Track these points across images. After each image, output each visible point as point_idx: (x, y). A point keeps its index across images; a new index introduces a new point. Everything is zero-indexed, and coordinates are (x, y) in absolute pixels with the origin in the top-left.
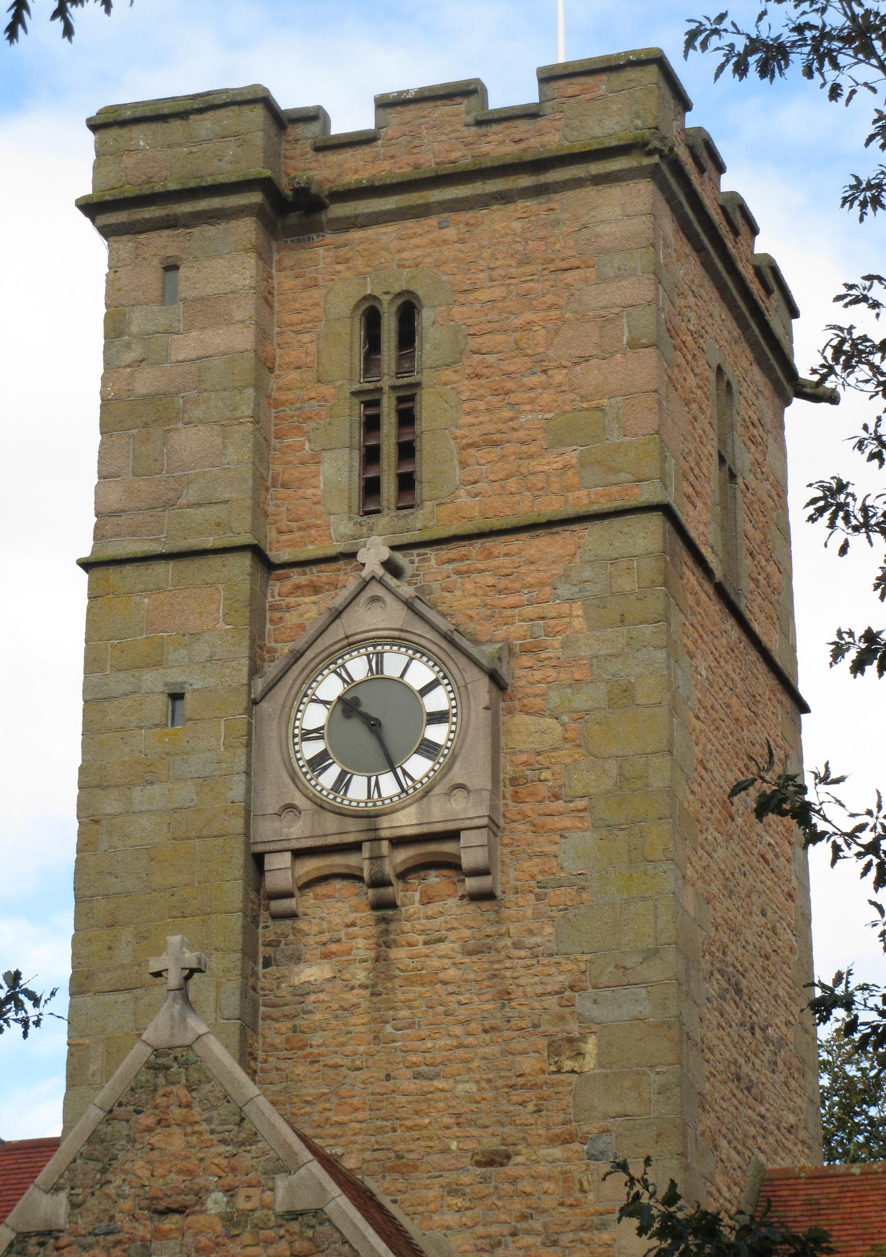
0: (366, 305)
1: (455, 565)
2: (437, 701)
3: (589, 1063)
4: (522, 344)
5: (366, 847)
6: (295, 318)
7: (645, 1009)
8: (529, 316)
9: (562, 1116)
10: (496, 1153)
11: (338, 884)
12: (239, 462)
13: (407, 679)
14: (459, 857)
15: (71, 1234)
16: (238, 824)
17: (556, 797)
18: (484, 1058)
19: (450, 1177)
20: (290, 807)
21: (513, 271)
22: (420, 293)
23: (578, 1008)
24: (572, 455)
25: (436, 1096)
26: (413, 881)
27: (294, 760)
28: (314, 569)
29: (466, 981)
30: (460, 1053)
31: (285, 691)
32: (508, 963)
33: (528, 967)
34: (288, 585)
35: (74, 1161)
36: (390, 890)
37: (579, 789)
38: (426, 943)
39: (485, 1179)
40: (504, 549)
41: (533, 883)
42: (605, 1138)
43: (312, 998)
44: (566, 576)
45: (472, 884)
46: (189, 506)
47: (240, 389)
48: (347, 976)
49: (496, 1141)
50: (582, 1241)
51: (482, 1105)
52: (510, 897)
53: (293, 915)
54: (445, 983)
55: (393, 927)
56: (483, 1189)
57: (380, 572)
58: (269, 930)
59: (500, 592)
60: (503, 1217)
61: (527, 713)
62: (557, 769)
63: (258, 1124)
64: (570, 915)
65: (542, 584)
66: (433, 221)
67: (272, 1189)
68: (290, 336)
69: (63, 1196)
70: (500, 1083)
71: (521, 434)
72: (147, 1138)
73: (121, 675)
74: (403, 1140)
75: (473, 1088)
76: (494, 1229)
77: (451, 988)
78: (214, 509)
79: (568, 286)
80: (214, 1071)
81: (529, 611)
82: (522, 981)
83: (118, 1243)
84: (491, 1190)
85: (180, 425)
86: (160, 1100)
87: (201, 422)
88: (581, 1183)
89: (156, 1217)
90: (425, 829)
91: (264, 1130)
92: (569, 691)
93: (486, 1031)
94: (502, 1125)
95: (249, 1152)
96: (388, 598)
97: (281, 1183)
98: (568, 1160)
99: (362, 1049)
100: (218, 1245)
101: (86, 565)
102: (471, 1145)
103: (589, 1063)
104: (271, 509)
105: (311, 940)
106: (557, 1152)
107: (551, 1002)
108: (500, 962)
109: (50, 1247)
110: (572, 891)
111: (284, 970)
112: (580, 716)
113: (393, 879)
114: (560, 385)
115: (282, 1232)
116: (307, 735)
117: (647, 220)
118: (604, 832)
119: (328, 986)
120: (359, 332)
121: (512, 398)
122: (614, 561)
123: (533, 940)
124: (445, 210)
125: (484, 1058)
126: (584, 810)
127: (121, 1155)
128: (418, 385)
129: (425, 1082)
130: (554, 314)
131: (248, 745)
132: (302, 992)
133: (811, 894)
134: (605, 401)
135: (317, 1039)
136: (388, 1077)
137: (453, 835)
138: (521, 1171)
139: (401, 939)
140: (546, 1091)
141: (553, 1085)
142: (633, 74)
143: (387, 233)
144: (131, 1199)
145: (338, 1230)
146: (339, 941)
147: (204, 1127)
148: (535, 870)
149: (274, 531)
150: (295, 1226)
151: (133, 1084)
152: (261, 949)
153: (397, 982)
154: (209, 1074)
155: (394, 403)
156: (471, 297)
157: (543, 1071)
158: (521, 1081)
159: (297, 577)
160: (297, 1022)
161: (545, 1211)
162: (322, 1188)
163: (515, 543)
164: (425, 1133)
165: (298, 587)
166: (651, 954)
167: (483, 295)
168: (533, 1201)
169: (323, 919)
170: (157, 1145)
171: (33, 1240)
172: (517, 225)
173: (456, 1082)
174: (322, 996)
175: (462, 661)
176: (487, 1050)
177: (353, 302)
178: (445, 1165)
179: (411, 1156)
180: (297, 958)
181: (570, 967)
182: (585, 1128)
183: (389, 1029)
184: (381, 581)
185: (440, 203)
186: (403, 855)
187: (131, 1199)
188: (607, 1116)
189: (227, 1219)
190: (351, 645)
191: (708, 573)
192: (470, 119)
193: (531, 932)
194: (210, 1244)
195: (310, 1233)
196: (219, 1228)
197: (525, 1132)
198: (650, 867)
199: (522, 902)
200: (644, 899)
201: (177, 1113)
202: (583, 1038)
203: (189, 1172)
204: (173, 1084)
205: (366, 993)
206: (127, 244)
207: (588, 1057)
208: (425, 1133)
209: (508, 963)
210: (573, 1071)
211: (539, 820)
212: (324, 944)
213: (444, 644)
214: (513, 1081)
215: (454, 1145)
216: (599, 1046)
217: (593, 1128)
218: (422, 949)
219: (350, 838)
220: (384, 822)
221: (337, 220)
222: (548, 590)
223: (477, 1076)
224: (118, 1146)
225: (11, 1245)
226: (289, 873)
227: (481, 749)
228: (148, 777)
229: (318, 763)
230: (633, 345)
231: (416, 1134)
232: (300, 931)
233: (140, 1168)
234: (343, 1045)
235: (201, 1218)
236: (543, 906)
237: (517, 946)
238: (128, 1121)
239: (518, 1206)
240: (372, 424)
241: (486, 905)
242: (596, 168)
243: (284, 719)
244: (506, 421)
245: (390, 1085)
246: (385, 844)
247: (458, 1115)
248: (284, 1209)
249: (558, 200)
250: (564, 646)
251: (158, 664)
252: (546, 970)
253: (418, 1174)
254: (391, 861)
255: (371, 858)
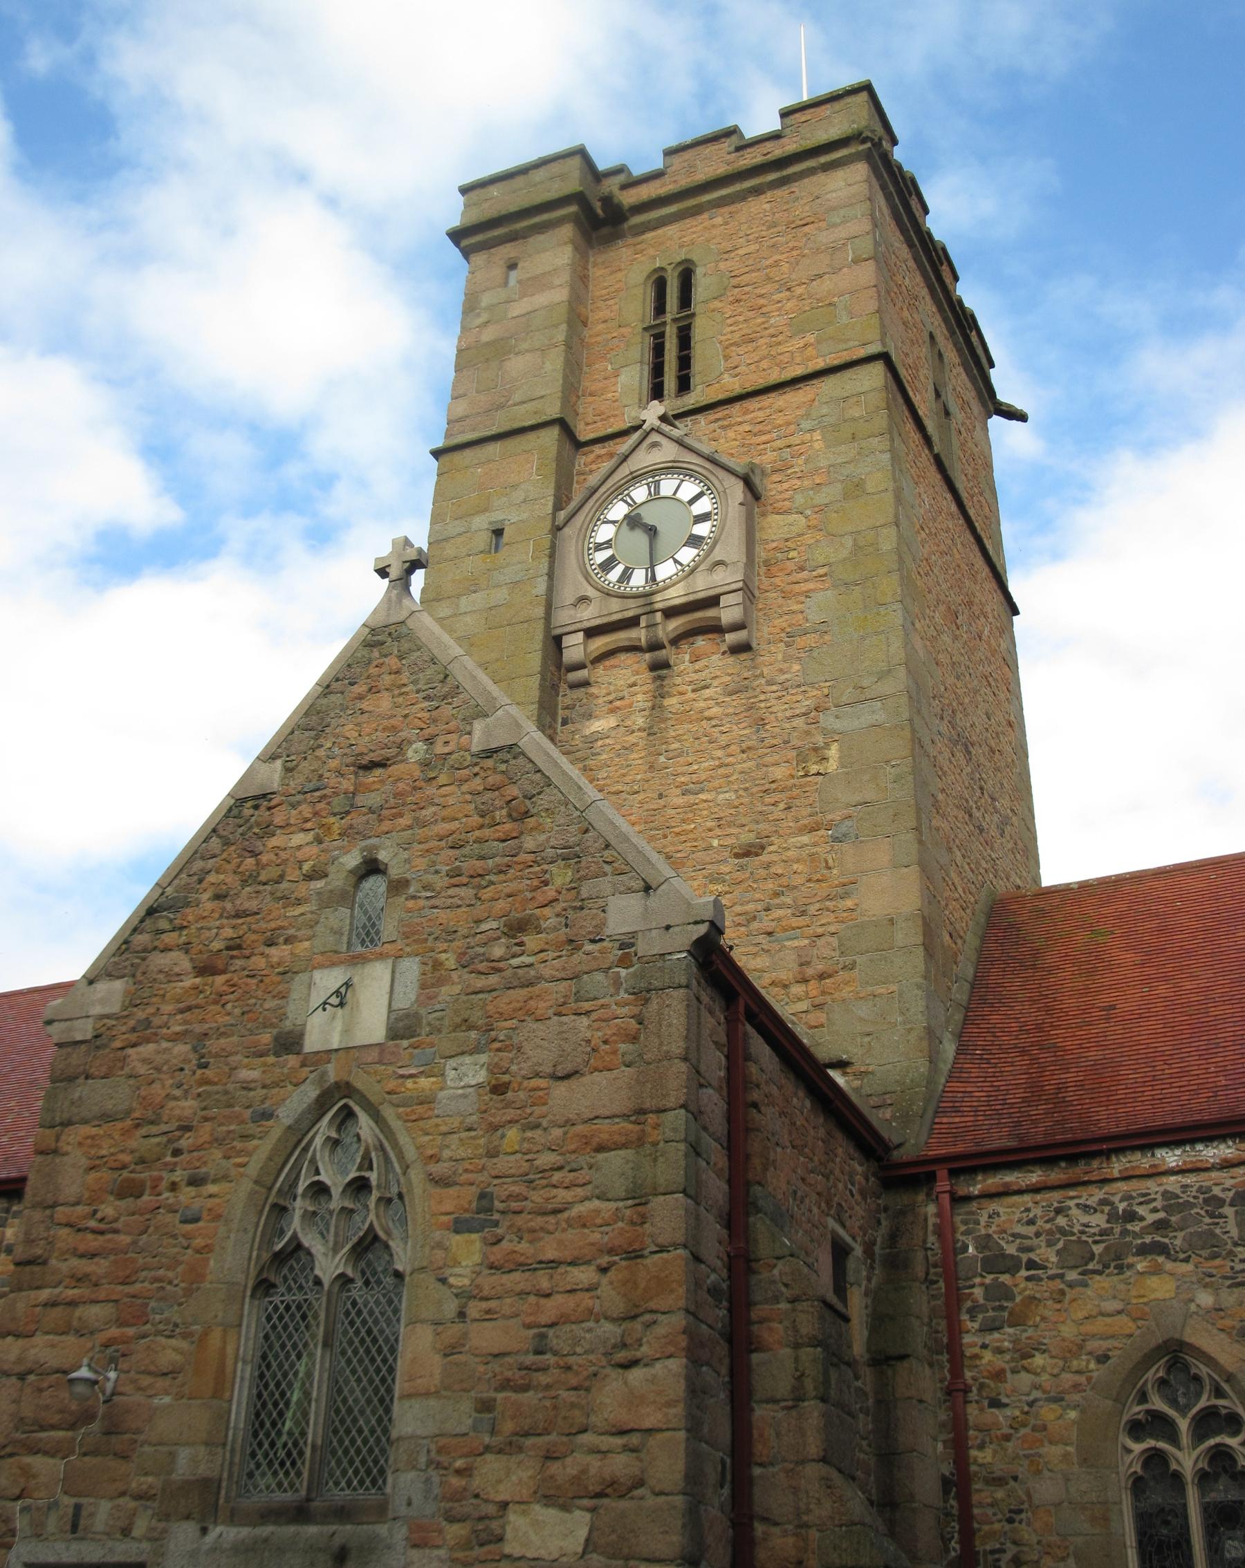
0: (656, 276)
1: (720, 423)
2: (704, 506)
3: (832, 766)
4: (771, 275)
5: (643, 622)
6: (604, 292)
7: (880, 717)
8: (777, 257)
9: (809, 810)
10: (751, 845)
11: (623, 657)
12: (554, 370)
13: (678, 495)
14: (720, 619)
15: (283, 795)
16: (540, 611)
17: (802, 569)
18: (741, 773)
19: (711, 869)
20: (584, 599)
21: (764, 233)
22: (695, 259)
23: (822, 724)
24: (811, 338)
25: (701, 806)
26: (684, 646)
27: (588, 566)
28: (611, 443)
29: (727, 715)
30: (722, 771)
31: (582, 518)
32: (762, 697)
33: (779, 698)
34: (592, 457)
35: (292, 732)
36: (664, 651)
37: (821, 560)
38: (693, 691)
39: (742, 868)
40: (758, 406)
41: (783, 635)
42: (848, 823)
43: (600, 743)
44: (807, 415)
45: (731, 638)
46: (515, 405)
47: (556, 326)
48: (628, 723)
49: (752, 835)
50: (828, 910)
51: (741, 809)
52: (764, 646)
53: (586, 684)
54: (710, 719)
55: (665, 683)
56: (740, 876)
57: (658, 423)
58: (566, 697)
59: (755, 435)
60: (757, 896)
61: (778, 513)
62: (803, 548)
63: (460, 679)
64: (815, 654)
65: (788, 424)
66: (706, 216)
67: (469, 733)
68: (601, 304)
69: (278, 764)
70: (755, 789)
71: (772, 331)
72: (360, 705)
73: (457, 522)
74: (673, 844)
75: (732, 796)
76: (750, 907)
77: (713, 722)
78: (533, 403)
79: (806, 235)
80: (423, 639)
81: (779, 443)
82: (773, 709)
83: (324, 796)
84: (748, 875)
85: (512, 356)
86: (373, 671)
87: (527, 351)
88: (826, 862)
89: (361, 773)
90: (691, 598)
91: (467, 684)
92: (811, 492)
93: (743, 752)
94: (758, 823)
95: (450, 704)
96: (663, 441)
97: (478, 726)
98: (815, 845)
99: (639, 777)
100: (415, 788)
101: (437, 454)
102: (729, 841)
103: (832, 766)
104: (581, 410)
105: (601, 701)
106: (805, 839)
107: (800, 722)
108: (756, 697)
109: (263, 808)
110: (816, 636)
111: (578, 726)
112: (820, 509)
113: (666, 644)
114: (801, 295)
115: (477, 769)
116: (599, 547)
117: (865, 186)
118: (843, 589)
119: (613, 733)
120: (651, 294)
121: (764, 310)
122: (845, 399)
123: (783, 678)
124: (714, 207)
125: (741, 773)
126: (825, 575)
127: (334, 722)
128: (693, 315)
129: (691, 797)
130: (795, 253)
131: (552, 556)
132: (591, 740)
133: (1030, 760)
134: (836, 299)
135: (602, 774)
136: (661, 796)
137: (713, 601)
138: (775, 857)
139: (674, 691)
140: (795, 792)
141: (801, 786)
142: (849, 100)
143: (671, 230)
144: (339, 758)
145: (531, 761)
146: (622, 698)
147: (411, 687)
148: (784, 625)
149: (582, 423)
150: (489, 763)
151: (350, 661)
152: (560, 712)
153: (670, 723)
154: (418, 642)
155: (675, 331)
156: (732, 255)
157: (792, 776)
158: (773, 786)
159: (598, 450)
160: (587, 763)
161: (795, 887)
162: (518, 726)
163: (767, 400)
164: (691, 836)
165: (599, 456)
166: (882, 676)
167: (741, 252)
168: (784, 881)
169: (610, 684)
170: (366, 709)
171: (250, 804)
172: (767, 206)
173: (718, 793)
174: (607, 741)
175: (721, 474)
176: (744, 765)
177: (645, 274)
178: (708, 859)
179: (679, 855)
180: (589, 716)
181: (815, 693)
182: (829, 817)
183: (662, 759)
184: (658, 431)
185: (709, 202)
186: (675, 625)
187: (339, 758)
188: (848, 805)
189: (425, 764)
190: (635, 478)
191: (927, 440)
192: (732, 149)
193: (781, 671)
194: (408, 788)
195: (503, 767)
196: (417, 773)
197: (776, 826)
198: (882, 609)
199: (773, 649)
200: (877, 633)
201: (387, 679)
202: (827, 746)
203: (394, 729)
204: (386, 656)
205: (644, 734)
206: (479, 259)
207: (831, 761)
208: (691, 836)
209: (762, 697)
210: (819, 774)
211: (788, 588)
212: (611, 702)
213: (708, 465)
214: (767, 786)
215: (715, 843)
216: (840, 750)
217: (837, 816)
218: (691, 695)
219: (630, 614)
220: (658, 597)
221: (636, 226)
222: (793, 427)
223: (736, 787)
224: (332, 715)
225: (230, 810)
226: (582, 647)
227: (735, 534)
228: (473, 588)
229: (607, 565)
230: (856, 261)
231: (683, 838)
232: (591, 695)
233: (349, 731)
234: (624, 776)
235: (401, 767)
236: (791, 651)
237: (770, 683)
238: (342, 693)
239: (771, 886)
240: (659, 350)
241: (743, 656)
242: (823, 159)
243: (581, 537)
244: (759, 325)
245: (662, 802)
246: (659, 615)
247: (719, 819)
248: (480, 748)
249: (795, 187)
250: (807, 462)
251: (486, 510)
252: (795, 698)
253: (685, 869)
254: (664, 629)
255: (647, 627)
